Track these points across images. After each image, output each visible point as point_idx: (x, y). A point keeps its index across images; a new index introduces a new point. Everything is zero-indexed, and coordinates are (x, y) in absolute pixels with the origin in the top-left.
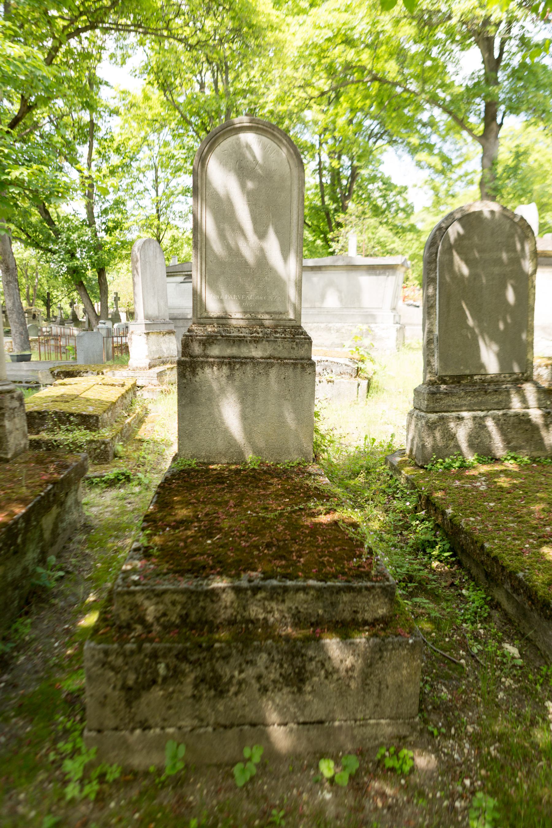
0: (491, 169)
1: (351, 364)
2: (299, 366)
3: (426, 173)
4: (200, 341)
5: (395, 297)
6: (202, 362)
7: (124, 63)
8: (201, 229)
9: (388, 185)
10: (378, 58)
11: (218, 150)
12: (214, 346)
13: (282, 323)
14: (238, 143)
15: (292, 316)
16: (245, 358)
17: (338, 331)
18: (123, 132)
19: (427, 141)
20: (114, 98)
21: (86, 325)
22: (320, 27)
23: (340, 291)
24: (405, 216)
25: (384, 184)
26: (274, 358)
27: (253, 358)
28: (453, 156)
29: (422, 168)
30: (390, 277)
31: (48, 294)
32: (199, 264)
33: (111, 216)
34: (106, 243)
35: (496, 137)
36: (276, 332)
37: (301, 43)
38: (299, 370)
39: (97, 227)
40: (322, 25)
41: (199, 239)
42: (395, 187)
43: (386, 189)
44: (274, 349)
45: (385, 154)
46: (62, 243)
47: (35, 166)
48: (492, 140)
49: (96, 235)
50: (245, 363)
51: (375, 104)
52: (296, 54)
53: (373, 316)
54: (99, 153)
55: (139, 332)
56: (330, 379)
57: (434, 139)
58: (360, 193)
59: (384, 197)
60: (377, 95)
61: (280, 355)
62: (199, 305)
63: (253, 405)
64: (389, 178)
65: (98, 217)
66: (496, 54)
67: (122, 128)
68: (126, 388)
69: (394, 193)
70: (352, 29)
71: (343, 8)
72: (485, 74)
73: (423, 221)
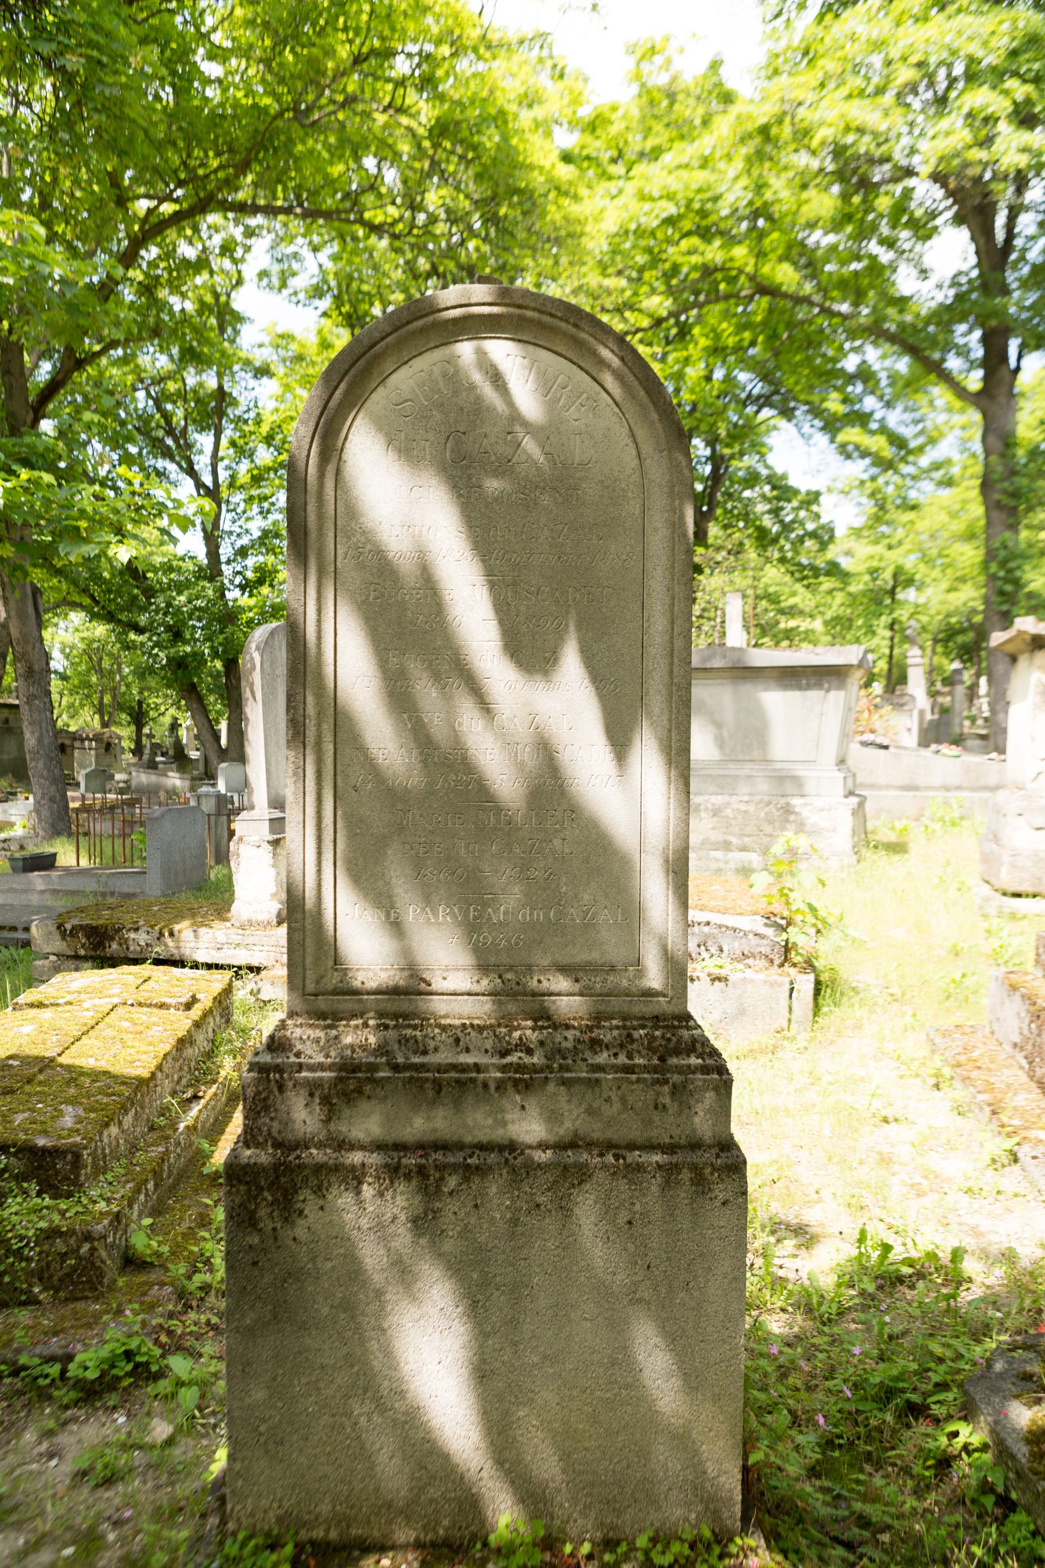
0: (1003, 456)
1: (770, 932)
2: (686, 1175)
3: (859, 468)
4: (312, 1088)
5: (845, 736)
6: (319, 1168)
7: (284, 285)
8: (319, 675)
9: (782, 490)
10: (765, 255)
11: (379, 399)
12: (364, 1105)
13: (616, 1004)
14: (454, 377)
15: (654, 978)
16: (483, 1147)
17: (716, 812)
18: (282, 407)
19: (857, 407)
20: (261, 346)
21: (201, 766)
22: (652, 199)
23: (718, 725)
24: (816, 547)
25: (774, 488)
26: (590, 1145)
27: (512, 1147)
28: (907, 432)
29: (848, 457)
30: (833, 694)
31: (140, 703)
32: (311, 799)
33: (251, 561)
34: (242, 610)
35: (1011, 395)
36: (595, 1044)
37: (614, 229)
38: (683, 1193)
39: (226, 581)
40: (656, 194)
41: (311, 710)
42: (796, 492)
43: (778, 499)
44: (590, 1112)
45: (774, 433)
46: (157, 612)
47: (25, 474)
48: (1002, 399)
49: (223, 595)
50: (481, 1171)
51: (761, 338)
52: (605, 248)
53: (797, 781)
54: (233, 444)
55: (255, 838)
56: (717, 971)
57: (870, 403)
58: (729, 506)
59: (776, 512)
60: (765, 323)
61: (611, 1134)
62: (310, 949)
63: (513, 1323)
64: (784, 477)
65: (228, 562)
66: (1000, 235)
67: (280, 399)
68: (196, 1012)
69: (795, 503)
70: (716, 199)
71: (695, 163)
72: (980, 276)
73: (848, 553)
